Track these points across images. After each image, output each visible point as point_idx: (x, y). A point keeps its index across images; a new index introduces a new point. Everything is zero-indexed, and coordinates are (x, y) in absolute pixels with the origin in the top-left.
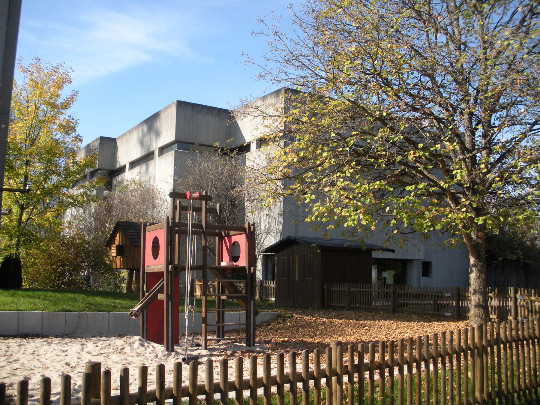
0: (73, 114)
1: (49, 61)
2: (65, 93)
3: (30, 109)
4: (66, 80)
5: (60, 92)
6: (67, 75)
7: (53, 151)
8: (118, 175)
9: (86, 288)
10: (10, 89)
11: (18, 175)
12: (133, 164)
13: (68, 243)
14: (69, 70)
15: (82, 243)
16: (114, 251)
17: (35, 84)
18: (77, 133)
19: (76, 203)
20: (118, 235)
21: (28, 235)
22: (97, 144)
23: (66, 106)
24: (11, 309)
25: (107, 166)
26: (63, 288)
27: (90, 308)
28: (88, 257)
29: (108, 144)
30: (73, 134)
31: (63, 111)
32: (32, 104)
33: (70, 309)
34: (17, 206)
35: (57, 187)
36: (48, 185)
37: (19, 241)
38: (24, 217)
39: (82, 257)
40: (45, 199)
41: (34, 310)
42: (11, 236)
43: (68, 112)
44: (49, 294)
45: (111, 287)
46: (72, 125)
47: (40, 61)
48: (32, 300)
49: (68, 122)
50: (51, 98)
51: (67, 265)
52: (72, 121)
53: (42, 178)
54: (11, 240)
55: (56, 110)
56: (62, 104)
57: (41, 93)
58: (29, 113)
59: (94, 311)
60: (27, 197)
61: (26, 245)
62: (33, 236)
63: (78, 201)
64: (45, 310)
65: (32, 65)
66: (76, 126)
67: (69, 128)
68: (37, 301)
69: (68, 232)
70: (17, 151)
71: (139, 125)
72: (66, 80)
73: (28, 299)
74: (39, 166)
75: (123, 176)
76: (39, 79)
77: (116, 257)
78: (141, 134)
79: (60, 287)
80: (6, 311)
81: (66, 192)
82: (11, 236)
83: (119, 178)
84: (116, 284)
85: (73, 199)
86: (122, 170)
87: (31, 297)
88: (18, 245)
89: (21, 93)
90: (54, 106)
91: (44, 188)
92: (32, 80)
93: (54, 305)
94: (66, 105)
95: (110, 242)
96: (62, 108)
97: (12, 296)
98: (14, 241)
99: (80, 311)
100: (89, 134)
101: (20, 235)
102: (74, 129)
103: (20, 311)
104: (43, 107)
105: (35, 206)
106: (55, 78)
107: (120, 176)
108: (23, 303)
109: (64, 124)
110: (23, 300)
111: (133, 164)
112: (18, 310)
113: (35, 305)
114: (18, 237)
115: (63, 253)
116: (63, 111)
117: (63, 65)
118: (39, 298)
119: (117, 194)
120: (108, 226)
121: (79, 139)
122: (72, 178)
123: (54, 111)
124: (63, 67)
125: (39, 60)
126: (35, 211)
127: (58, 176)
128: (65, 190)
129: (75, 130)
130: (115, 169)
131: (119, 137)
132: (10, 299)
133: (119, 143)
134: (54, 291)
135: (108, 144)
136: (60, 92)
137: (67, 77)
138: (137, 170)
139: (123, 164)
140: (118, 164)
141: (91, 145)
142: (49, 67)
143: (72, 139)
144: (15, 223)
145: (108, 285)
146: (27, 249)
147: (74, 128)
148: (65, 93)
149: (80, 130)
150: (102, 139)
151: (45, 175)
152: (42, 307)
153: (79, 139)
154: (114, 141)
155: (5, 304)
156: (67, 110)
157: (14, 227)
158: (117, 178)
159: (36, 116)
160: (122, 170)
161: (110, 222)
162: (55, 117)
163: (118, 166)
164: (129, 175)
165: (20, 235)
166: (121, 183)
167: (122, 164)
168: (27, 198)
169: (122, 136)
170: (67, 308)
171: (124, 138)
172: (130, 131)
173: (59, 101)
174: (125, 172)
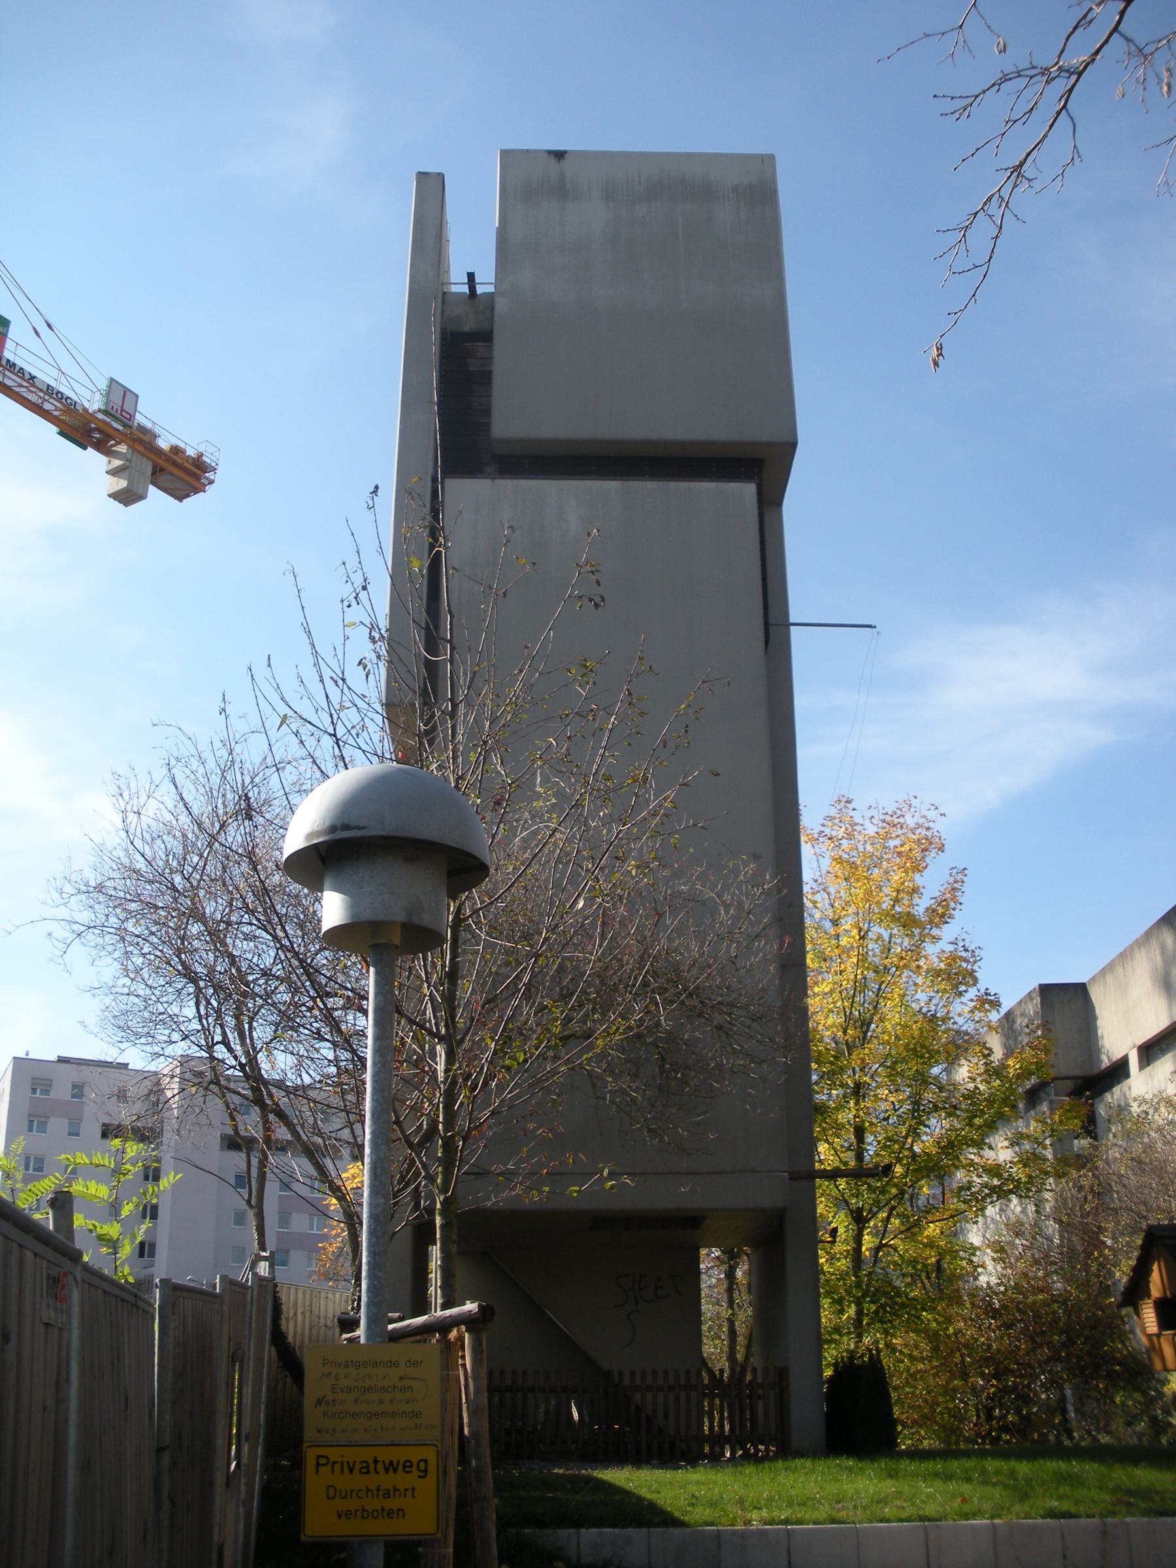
0: (964, 936)
1: (873, 801)
2: (932, 883)
3: (844, 941)
4: (930, 844)
5: (919, 879)
6: (928, 829)
7: (929, 1045)
8: (1109, 1087)
9: (1057, 1436)
10: (800, 894)
11: (840, 1127)
12: (1150, 1051)
13: (1004, 1307)
14: (932, 815)
15: (1045, 1303)
16: (1149, 1318)
17: (850, 870)
18: (982, 986)
19: (1003, 1187)
20: (1155, 1267)
21: (886, 1294)
22: (1032, 1008)
23: (943, 916)
24: (903, 1515)
25: (1067, 1064)
26: (1007, 1442)
27: (1128, 1504)
28: (1070, 1343)
29: (1067, 1004)
30: (972, 993)
31: (934, 932)
32: (848, 927)
33: (1073, 1510)
34: (842, 1214)
35: (951, 1147)
36: (926, 1143)
37: (860, 1313)
38: (868, 1241)
39: (1050, 1344)
40: (917, 1186)
41: (966, 1516)
42: (840, 1301)
43: (947, 932)
44: (991, 1465)
45: (1138, 1429)
46: (964, 965)
47: (850, 806)
48: (952, 1486)
49: (953, 958)
50: (896, 901)
51: (1012, 1371)
52: (964, 954)
53: (904, 1130)
54: (842, 1311)
55: (917, 931)
56: (931, 911)
57: (869, 892)
58: (846, 951)
59: (1147, 1513)
60: (869, 1186)
61: (882, 1322)
62: (900, 1296)
63: (1013, 1180)
64: (999, 1516)
65: (832, 818)
66: (976, 968)
67: (957, 974)
68: (966, 1488)
69: (990, 1274)
70: (832, 1063)
71: (1148, 935)
72: (930, 844)
73: (939, 1484)
74: (886, 1099)
75: (1125, 1089)
76: (854, 853)
77: (1158, 1336)
78: (1159, 959)
79: (998, 1438)
80: (888, 1521)
81: (977, 1159)
82: (840, 1301)
83: (1114, 1096)
84: (1154, 1420)
85: (999, 1175)
86: (1119, 1070)
87: (948, 1477)
88: (858, 1322)
89: (814, 902)
90: (908, 922)
91: (914, 1156)
92: (839, 860)
93: (1021, 1500)
94: (941, 914)
95: (1135, 1291)
96: (931, 922)
97: (890, 1476)
98: (852, 1311)
99: (1102, 1516)
100: (1010, 981)
101: (863, 1296)
102: (970, 977)
103: (929, 1520)
104: (876, 929)
105: (893, 1208)
106: (897, 842)
107: (1116, 1090)
108: (929, 1496)
109: (942, 966)
110: (926, 1489)
111: (1150, 1051)
112: (922, 1519)
113: (964, 1500)
114: (859, 1304)
115: (990, 1336)
116: (934, 932)
117: (913, 801)
118: (969, 1480)
119: (1114, 1148)
120: (1109, 1242)
121: (988, 1001)
122: (984, 1115)
123: (912, 936)
124: (912, 809)
125: (848, 802)
126: (896, 1222)
127: (949, 1115)
128: (971, 1154)
129: (976, 981)
130: (1096, 1071)
131: (1093, 978)
132: (888, 1486)
133: (1096, 994)
134: (1006, 1455)
135: (1067, 1004)
136: (919, 879)
137: (929, 834)
138: (1164, 1066)
139: (1120, 1056)
140: (1104, 1057)
141: (1017, 1013)
142: (879, 816)
143: (972, 1004)
144: (843, 1264)
145: (1129, 1424)
146: (886, 1333)
147: (971, 974)
148: (932, 883)
149: (988, 978)
150: (1046, 991)
151: (914, 1117)
152: (986, 1506)
153: (991, 1002)
154: (1079, 991)
155: (883, 1501)
156: (945, 927)
157: (843, 1277)
158: (1108, 1097)
159: (862, 959)
160: (1119, 1070)
161: (1114, 1233)
162: (916, 951)
163: (1105, 1063)
164: (1141, 1085)
165: (863, 1296)
166: (1122, 1109)
167: (1117, 1055)
168: (871, 1189)
169: (1103, 972)
170: (1066, 1506)
171: (1109, 979)
172: (1125, 956)
173: (921, 906)
174: (1128, 1076)
